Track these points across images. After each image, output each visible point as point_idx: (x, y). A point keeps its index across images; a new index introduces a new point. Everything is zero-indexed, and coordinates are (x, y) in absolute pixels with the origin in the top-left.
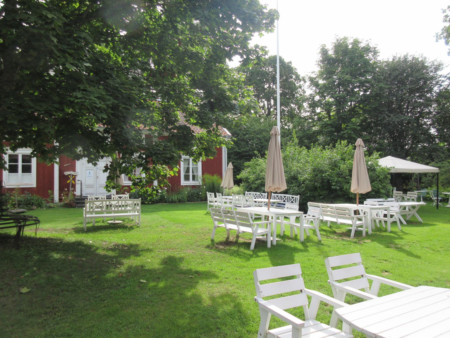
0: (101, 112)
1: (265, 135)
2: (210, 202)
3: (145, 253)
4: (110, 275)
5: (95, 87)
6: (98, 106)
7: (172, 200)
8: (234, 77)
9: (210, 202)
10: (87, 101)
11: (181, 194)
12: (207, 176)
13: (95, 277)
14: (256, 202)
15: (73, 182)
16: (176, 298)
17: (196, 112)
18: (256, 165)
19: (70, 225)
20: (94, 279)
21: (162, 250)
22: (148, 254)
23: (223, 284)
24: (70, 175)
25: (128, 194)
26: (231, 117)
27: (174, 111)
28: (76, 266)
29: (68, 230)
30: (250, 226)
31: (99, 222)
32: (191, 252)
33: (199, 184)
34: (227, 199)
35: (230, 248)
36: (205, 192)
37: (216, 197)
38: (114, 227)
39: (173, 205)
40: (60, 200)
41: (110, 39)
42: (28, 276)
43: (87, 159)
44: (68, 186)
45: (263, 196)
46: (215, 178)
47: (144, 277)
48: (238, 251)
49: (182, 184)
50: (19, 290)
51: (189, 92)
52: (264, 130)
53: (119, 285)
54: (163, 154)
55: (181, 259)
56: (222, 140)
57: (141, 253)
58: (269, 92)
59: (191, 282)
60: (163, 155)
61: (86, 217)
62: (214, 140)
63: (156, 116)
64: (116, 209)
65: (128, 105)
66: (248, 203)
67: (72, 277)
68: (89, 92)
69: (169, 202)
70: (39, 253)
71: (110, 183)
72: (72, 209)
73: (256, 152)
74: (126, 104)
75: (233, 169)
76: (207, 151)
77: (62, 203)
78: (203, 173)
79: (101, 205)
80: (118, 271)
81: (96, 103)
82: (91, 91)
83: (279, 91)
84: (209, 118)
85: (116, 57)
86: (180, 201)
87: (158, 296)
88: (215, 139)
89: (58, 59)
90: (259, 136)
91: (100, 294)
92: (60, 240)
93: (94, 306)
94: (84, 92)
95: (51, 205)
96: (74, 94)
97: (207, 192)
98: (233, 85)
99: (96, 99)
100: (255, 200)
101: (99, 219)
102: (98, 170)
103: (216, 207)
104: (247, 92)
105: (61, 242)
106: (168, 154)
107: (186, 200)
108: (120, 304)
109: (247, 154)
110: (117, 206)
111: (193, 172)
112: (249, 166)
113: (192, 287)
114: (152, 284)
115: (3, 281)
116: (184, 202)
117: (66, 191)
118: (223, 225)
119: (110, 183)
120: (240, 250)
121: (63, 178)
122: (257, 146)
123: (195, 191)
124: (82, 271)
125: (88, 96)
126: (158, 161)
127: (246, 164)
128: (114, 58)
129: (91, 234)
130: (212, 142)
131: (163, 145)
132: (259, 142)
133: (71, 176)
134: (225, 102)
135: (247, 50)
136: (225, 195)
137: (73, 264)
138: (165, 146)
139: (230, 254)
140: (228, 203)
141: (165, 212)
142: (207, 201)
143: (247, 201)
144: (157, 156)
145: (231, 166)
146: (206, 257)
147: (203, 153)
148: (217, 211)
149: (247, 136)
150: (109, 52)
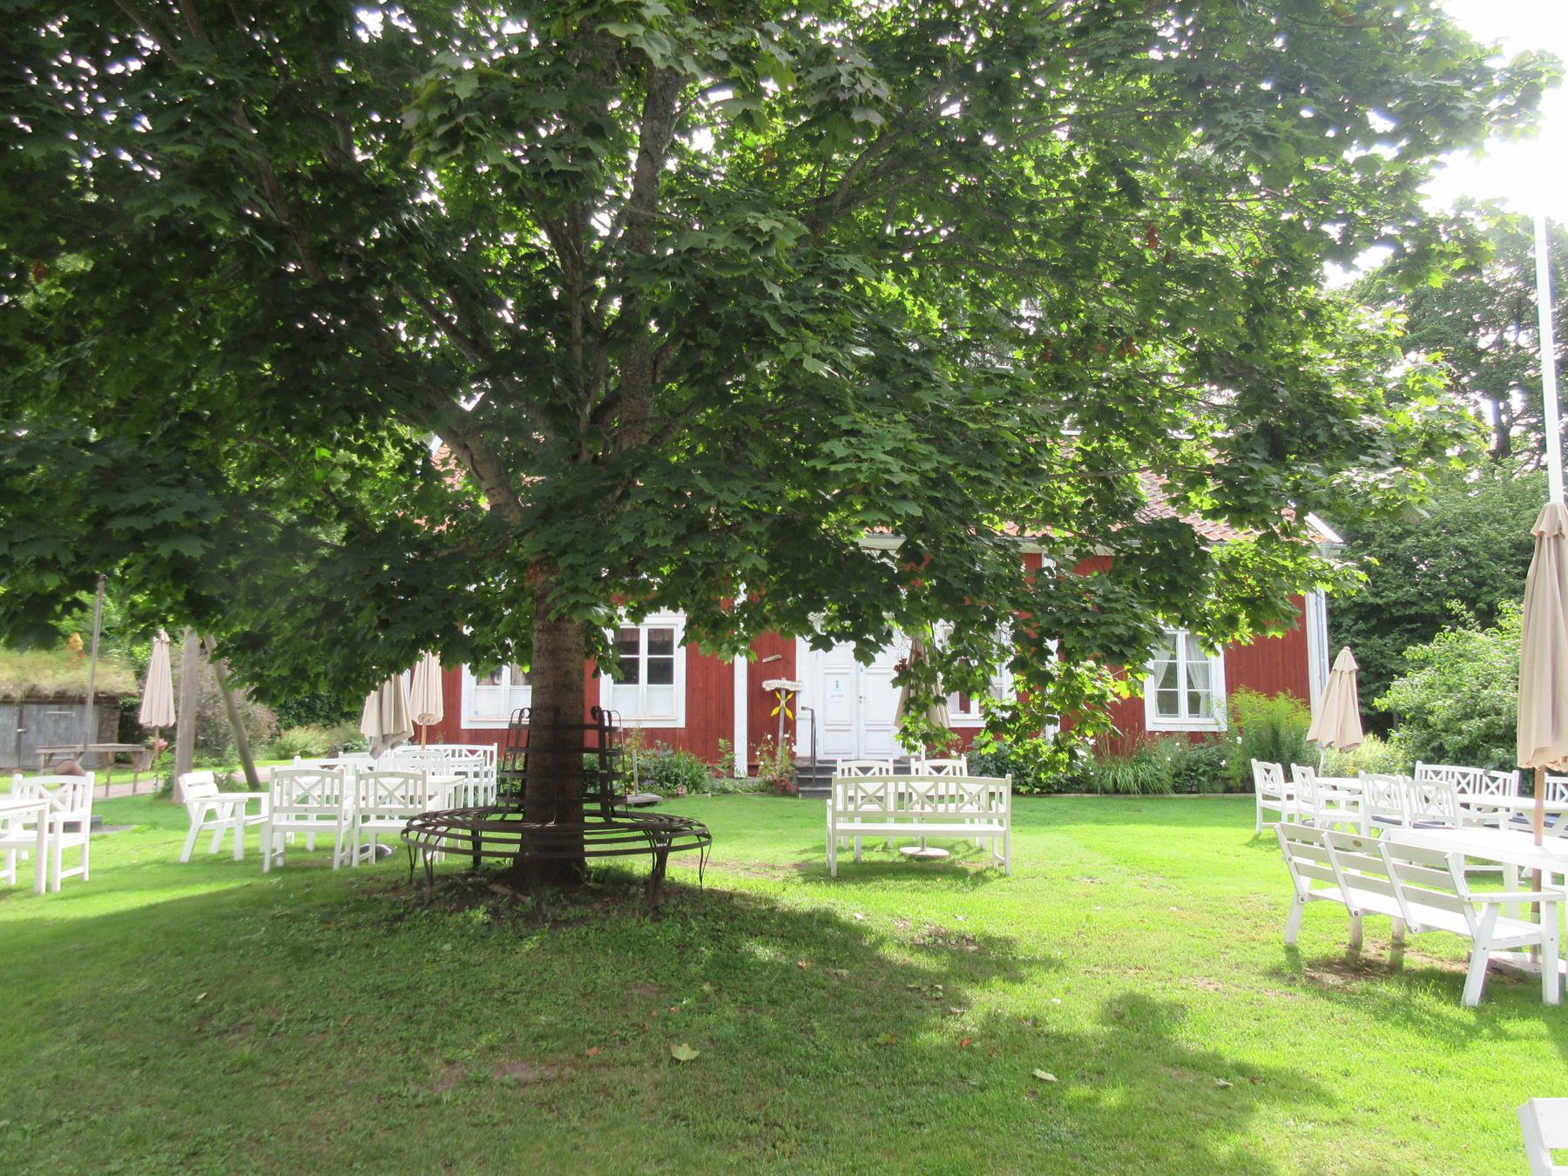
0: (904, 497)
1: (1493, 534)
2: (1266, 797)
3: (1038, 974)
4: (930, 1039)
5: (880, 417)
6: (896, 481)
7: (1115, 782)
8: (1361, 327)
9: (1266, 797)
10: (865, 466)
11: (1150, 761)
12: (1249, 700)
13: (883, 1038)
14: (1466, 806)
15: (789, 713)
16: (1173, 1159)
17: (1215, 472)
18: (1460, 656)
19: (787, 851)
20: (880, 1045)
21: (1098, 969)
22: (1050, 978)
23: (1359, 1133)
24: (779, 690)
25: (964, 758)
26: (1359, 479)
27: (1127, 470)
28: (822, 992)
29: (783, 868)
30: (1458, 905)
31: (872, 848)
32: (1211, 988)
33: (1215, 729)
34: (1335, 788)
35: (1372, 989)
36: (1241, 759)
37: (1288, 777)
38: (921, 869)
39: (1148, 805)
40: (753, 769)
41: (907, 256)
42: (688, 1010)
43: (852, 644)
44: (772, 724)
45: (1500, 782)
46: (1282, 704)
47: (1046, 1059)
48: (1406, 1002)
49: (1149, 727)
50: (668, 1049)
51: (1178, 398)
52: (1486, 517)
53: (963, 1078)
54: (1100, 624)
55: (1177, 1011)
56: (1318, 566)
57: (1024, 971)
58: (1498, 363)
59: (1222, 1104)
60: (1103, 630)
61: (836, 832)
62: (1285, 568)
63: (1068, 493)
64: (928, 809)
65: (986, 469)
66: (1433, 811)
67: (813, 1030)
68: (865, 436)
69: (1105, 791)
70: (716, 939)
71: (915, 720)
72: (786, 800)
73: (1455, 605)
74: (979, 467)
75: (1358, 672)
76: (1259, 607)
77: (758, 780)
78: (1231, 688)
79: (881, 794)
80: (954, 1026)
81: (889, 471)
82: (872, 432)
83: (1549, 355)
84: (1268, 489)
85: (922, 307)
86: (1145, 790)
87: (1105, 1138)
88: (1290, 565)
89: (782, 347)
90: (1463, 541)
91: (904, 1101)
92: (767, 901)
93: (890, 1140)
94: (853, 440)
95: (727, 783)
96: (825, 447)
97: (1254, 761)
98: (1358, 356)
99: (889, 459)
100: (1464, 798)
101: (867, 841)
103: (1291, 818)
104: (1418, 377)
105: (773, 909)
106: (1117, 624)
107: (1167, 787)
108: (973, 1147)
109: (1412, 611)
110: (931, 798)
111: (1190, 684)
112: (1423, 664)
113: (1232, 1125)
114: (1078, 1091)
115: (626, 1016)
116: (1161, 792)
117: (768, 742)
118: (1331, 892)
119: (915, 720)
120: (1417, 1001)
121: (760, 701)
122: (1456, 578)
123: (1202, 753)
124: (841, 1011)
125: (863, 450)
126: (1083, 650)
127: (1415, 651)
128: (917, 313)
129: (852, 887)
130: (1277, 575)
131: (1100, 592)
132: (1464, 562)
134: (1331, 426)
135: (1422, 225)
136: (1326, 774)
137: (813, 985)
138: (1106, 598)
139: (1375, 1013)
140: (1342, 804)
141: (1095, 827)
142: (1253, 790)
143: (1427, 800)
144: (1080, 634)
145: (1346, 659)
146: (1273, 1012)
147: (1242, 616)
148: (1304, 838)
149: (1410, 541)
150: (901, 294)
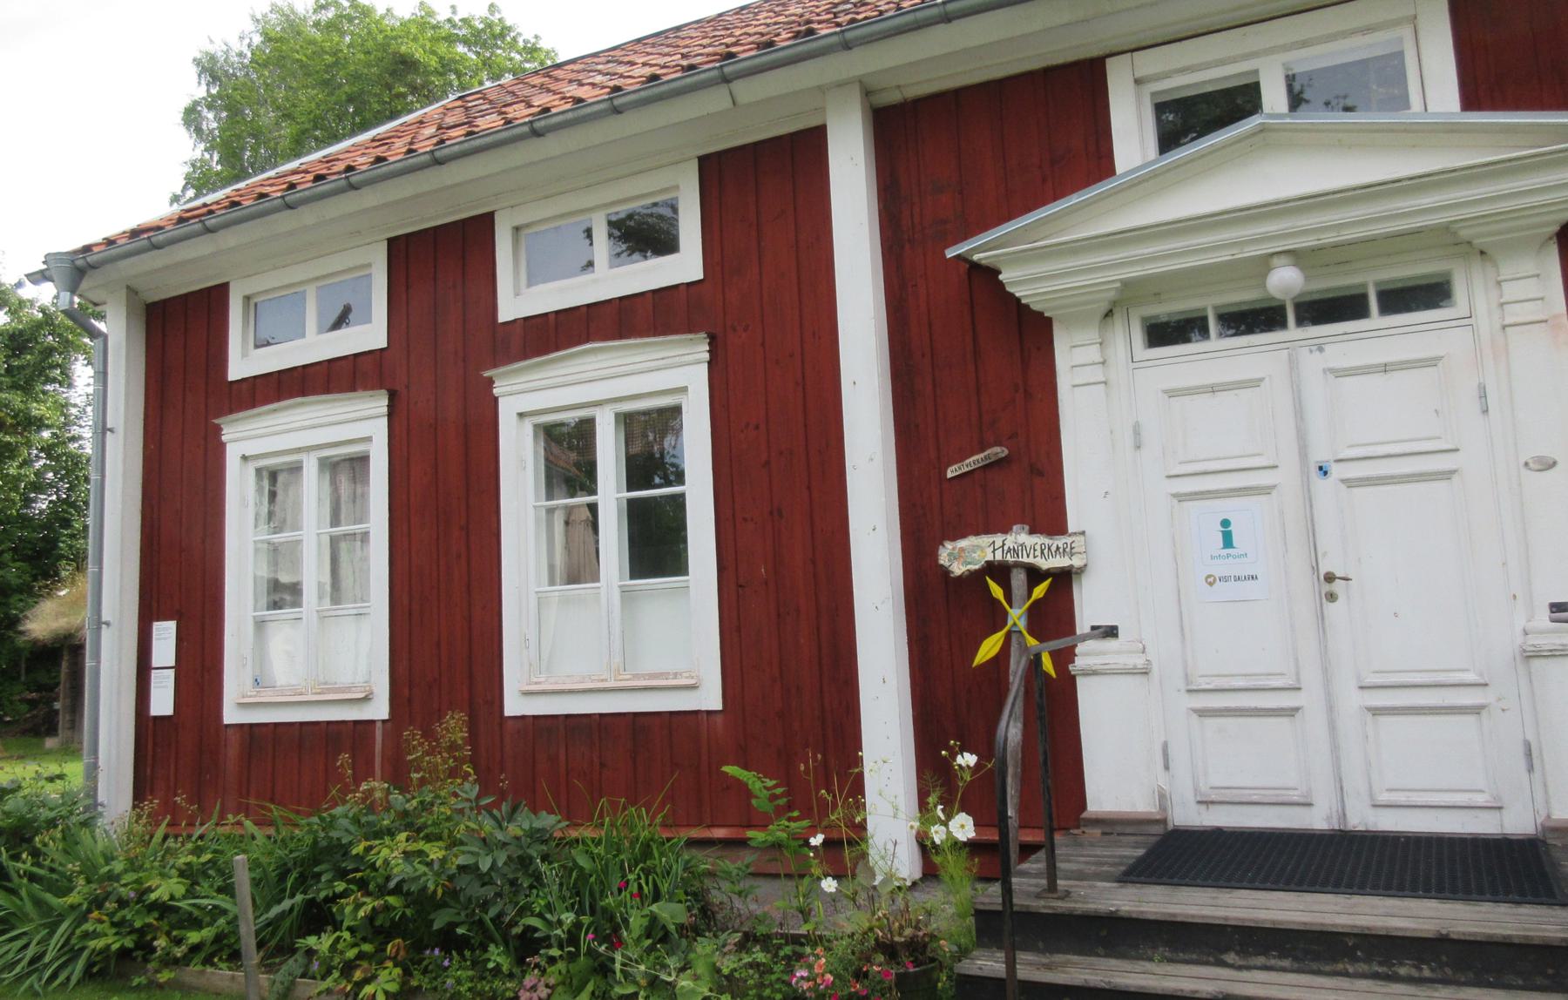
24: (999, 571)
133: (1018, 580)
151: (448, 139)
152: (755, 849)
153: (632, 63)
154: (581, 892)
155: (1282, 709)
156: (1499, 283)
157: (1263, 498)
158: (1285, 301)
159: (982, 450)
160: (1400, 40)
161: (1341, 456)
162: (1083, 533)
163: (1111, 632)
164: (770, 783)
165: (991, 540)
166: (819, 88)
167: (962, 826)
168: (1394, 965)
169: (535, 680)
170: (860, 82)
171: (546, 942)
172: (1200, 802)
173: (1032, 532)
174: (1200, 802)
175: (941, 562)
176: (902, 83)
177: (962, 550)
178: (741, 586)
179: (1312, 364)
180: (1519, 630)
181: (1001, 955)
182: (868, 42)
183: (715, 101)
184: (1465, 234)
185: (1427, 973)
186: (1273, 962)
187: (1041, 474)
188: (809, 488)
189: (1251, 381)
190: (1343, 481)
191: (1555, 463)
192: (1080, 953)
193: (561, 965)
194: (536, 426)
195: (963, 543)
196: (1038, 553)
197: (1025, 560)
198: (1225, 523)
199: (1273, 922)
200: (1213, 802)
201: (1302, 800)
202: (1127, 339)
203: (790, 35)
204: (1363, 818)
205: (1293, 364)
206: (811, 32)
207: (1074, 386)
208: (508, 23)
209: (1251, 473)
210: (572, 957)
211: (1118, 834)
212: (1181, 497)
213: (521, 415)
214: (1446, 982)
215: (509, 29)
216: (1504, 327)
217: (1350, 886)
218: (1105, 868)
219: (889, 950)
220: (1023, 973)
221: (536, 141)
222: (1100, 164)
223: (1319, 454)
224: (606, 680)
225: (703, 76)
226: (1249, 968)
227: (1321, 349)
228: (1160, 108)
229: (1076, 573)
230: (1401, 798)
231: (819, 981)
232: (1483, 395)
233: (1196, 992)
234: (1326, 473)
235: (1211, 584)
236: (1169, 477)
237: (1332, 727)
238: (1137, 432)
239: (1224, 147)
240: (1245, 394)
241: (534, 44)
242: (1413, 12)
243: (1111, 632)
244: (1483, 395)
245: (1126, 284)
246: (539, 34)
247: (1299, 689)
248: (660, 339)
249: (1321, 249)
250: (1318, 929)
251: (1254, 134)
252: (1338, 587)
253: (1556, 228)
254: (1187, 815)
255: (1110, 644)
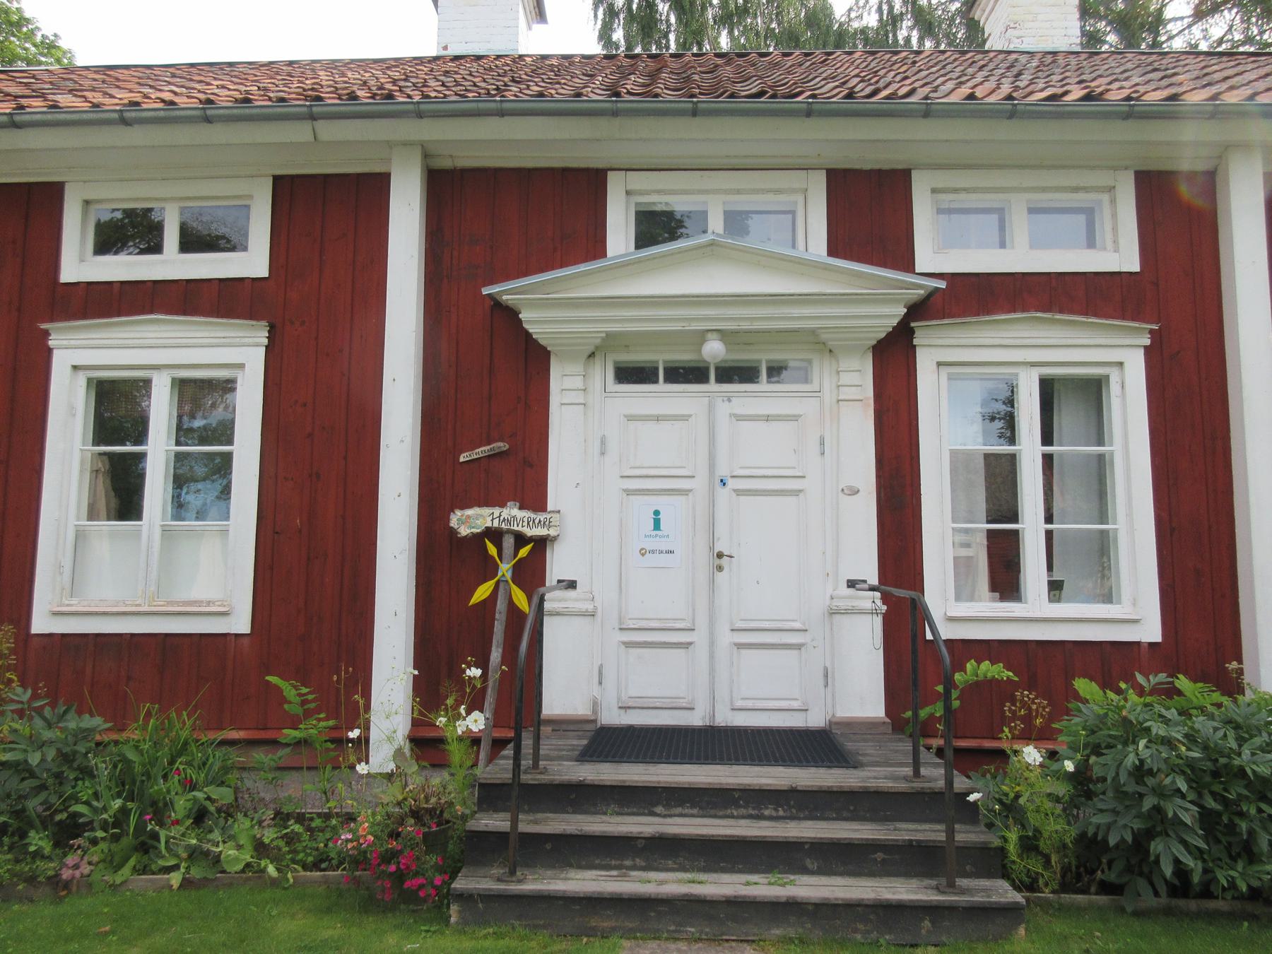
24: (494, 535)
102: (723, 494)
133: (508, 542)
151: (27, 107)
152: (287, 745)
153: (208, 84)
154: (126, 782)
155: (681, 643)
156: (838, 372)
157: (683, 498)
158: (709, 363)
159: (489, 445)
160: (796, 203)
161: (735, 474)
162: (559, 512)
163: (572, 585)
164: (304, 690)
165: (491, 511)
166: (388, 142)
167: (476, 721)
168: (762, 809)
169: (67, 602)
170: (422, 146)
171: (89, 826)
172: (620, 708)
173: (521, 508)
174: (620, 708)
175: (452, 525)
176: (454, 155)
177: (468, 517)
178: (277, 533)
179: (723, 409)
180: (828, 596)
181: (508, 815)
182: (437, 116)
183: (299, 133)
184: (824, 337)
185: (781, 813)
186: (686, 811)
187: (531, 466)
188: (345, 458)
189: (683, 416)
190: (735, 490)
191: (858, 491)
192: (555, 812)
193: (103, 846)
194: (89, 380)
195: (469, 512)
196: (525, 524)
197: (516, 528)
198: (657, 513)
199: (689, 783)
200: (629, 708)
201: (688, 706)
202: (602, 374)
203: (369, 95)
204: (726, 718)
205: (711, 409)
206: (390, 96)
207: (562, 404)
208: (27, 15)
209: (681, 480)
210: (116, 838)
211: (564, 731)
212: (629, 492)
213: (75, 368)
214: (792, 818)
215: (28, 21)
216: (838, 401)
217: (698, 758)
218: (564, 753)
219: (416, 814)
220: (524, 827)
221: (122, 130)
222: (596, 248)
223: (722, 471)
224: (140, 605)
225: (255, 111)
226: (671, 816)
227: (729, 400)
228: (638, 213)
229: (551, 541)
230: (749, 704)
231: (361, 841)
232: (822, 443)
233: (641, 833)
234: (724, 484)
235: (643, 555)
236: (622, 477)
237: (712, 656)
238: (603, 442)
239: (686, 251)
240: (678, 424)
241: (53, 41)
242: (805, 187)
243: (572, 585)
244: (822, 443)
245: (609, 336)
246: (59, 33)
247: (694, 630)
248: (224, 321)
249: (737, 332)
250: (718, 787)
251: (707, 246)
252: (725, 561)
253: (874, 342)
254: (612, 717)
255: (571, 594)
